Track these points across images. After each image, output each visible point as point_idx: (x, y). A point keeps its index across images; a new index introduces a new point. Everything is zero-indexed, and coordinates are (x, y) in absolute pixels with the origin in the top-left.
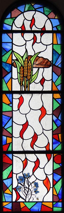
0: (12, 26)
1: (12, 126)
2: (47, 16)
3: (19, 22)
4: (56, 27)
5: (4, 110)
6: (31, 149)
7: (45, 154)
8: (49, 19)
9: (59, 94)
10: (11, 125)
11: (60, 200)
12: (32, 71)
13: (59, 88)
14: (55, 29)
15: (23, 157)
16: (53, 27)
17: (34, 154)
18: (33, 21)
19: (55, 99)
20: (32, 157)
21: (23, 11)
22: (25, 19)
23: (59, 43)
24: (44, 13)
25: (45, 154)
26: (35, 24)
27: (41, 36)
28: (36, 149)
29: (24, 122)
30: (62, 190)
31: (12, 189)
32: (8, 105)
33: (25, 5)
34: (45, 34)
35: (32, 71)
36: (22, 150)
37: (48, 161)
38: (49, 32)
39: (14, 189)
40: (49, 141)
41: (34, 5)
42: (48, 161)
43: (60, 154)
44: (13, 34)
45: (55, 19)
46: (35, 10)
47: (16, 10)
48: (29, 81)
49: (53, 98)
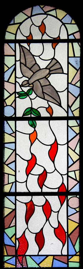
0: (16, 35)
1: (15, 161)
2: (61, 21)
3: (25, 30)
4: (73, 34)
5: (6, 140)
6: (38, 190)
7: (57, 196)
8: (64, 24)
9: (75, 120)
10: (47, 101)
11: (77, 253)
12: (49, 75)
13: (77, 114)
14: (71, 37)
15: (27, 199)
16: (68, 35)
17: (31, 191)
18: (42, 28)
19: (70, 127)
20: (39, 201)
21: (29, 15)
22: (33, 24)
23: (6, 176)
24: (56, 17)
25: (57, 196)
26: (46, 31)
27: (59, 36)
28: (45, 190)
29: (52, 141)
30: (79, 240)
31: (16, 239)
32: (10, 135)
33: (31, 8)
34: (60, 44)
35: (49, 75)
36: (27, 191)
37: (61, 206)
38: (63, 41)
39: (18, 239)
40: (27, 177)
41: (43, 7)
42: (61, 206)
43: (76, 197)
44: (16, 44)
45: (71, 24)
46: (45, 13)
47: (21, 14)
48: (47, 77)
49: (68, 126)
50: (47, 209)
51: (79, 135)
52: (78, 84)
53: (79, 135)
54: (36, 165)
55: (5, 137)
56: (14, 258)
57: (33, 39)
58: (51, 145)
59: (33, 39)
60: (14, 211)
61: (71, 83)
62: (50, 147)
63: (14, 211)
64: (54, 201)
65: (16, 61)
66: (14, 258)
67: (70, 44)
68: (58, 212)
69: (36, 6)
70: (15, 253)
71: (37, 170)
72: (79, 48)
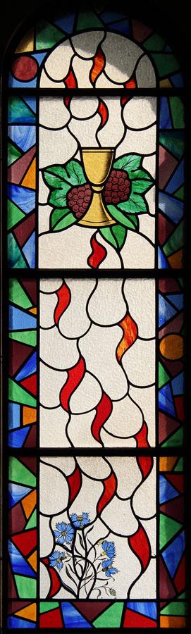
9: (101, 458)
15: (67, 465)
16: (158, 79)
20: (95, 468)
21: (70, 32)
50: (110, 487)
51: (182, 314)
52: (180, 194)
53: (182, 314)
54: (87, 373)
55: (11, 488)
56: (150, 183)
57: (79, 87)
58: (95, 408)
59: (79, 87)
60: (35, 491)
61: (163, 191)
62: (95, 411)
63: (35, 491)
64: (127, 469)
65: (37, 204)
66: (150, 183)
67: (164, 100)
68: (131, 498)
69: (57, 277)
70: (142, 87)
71: (86, 397)
72: (181, 107)
